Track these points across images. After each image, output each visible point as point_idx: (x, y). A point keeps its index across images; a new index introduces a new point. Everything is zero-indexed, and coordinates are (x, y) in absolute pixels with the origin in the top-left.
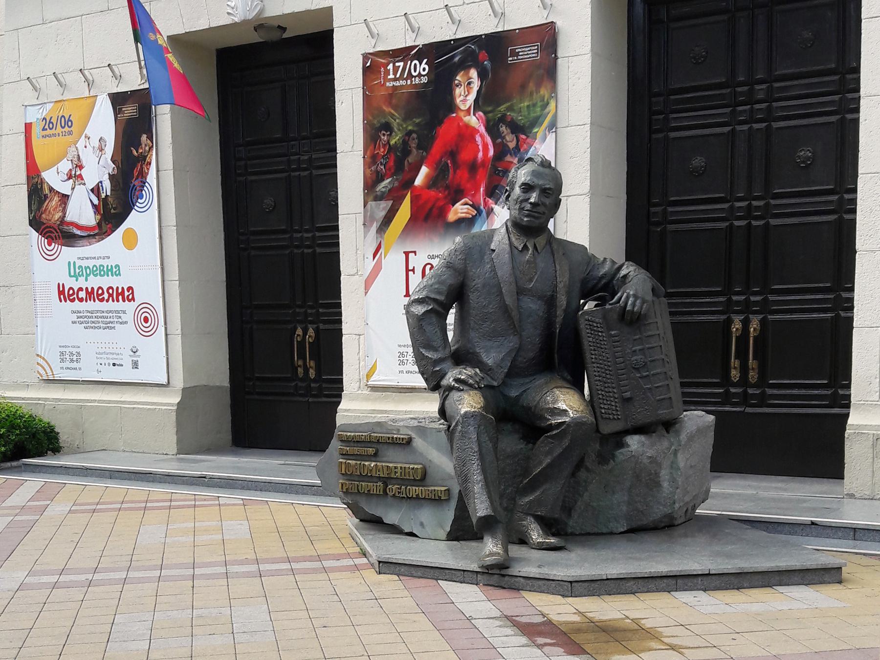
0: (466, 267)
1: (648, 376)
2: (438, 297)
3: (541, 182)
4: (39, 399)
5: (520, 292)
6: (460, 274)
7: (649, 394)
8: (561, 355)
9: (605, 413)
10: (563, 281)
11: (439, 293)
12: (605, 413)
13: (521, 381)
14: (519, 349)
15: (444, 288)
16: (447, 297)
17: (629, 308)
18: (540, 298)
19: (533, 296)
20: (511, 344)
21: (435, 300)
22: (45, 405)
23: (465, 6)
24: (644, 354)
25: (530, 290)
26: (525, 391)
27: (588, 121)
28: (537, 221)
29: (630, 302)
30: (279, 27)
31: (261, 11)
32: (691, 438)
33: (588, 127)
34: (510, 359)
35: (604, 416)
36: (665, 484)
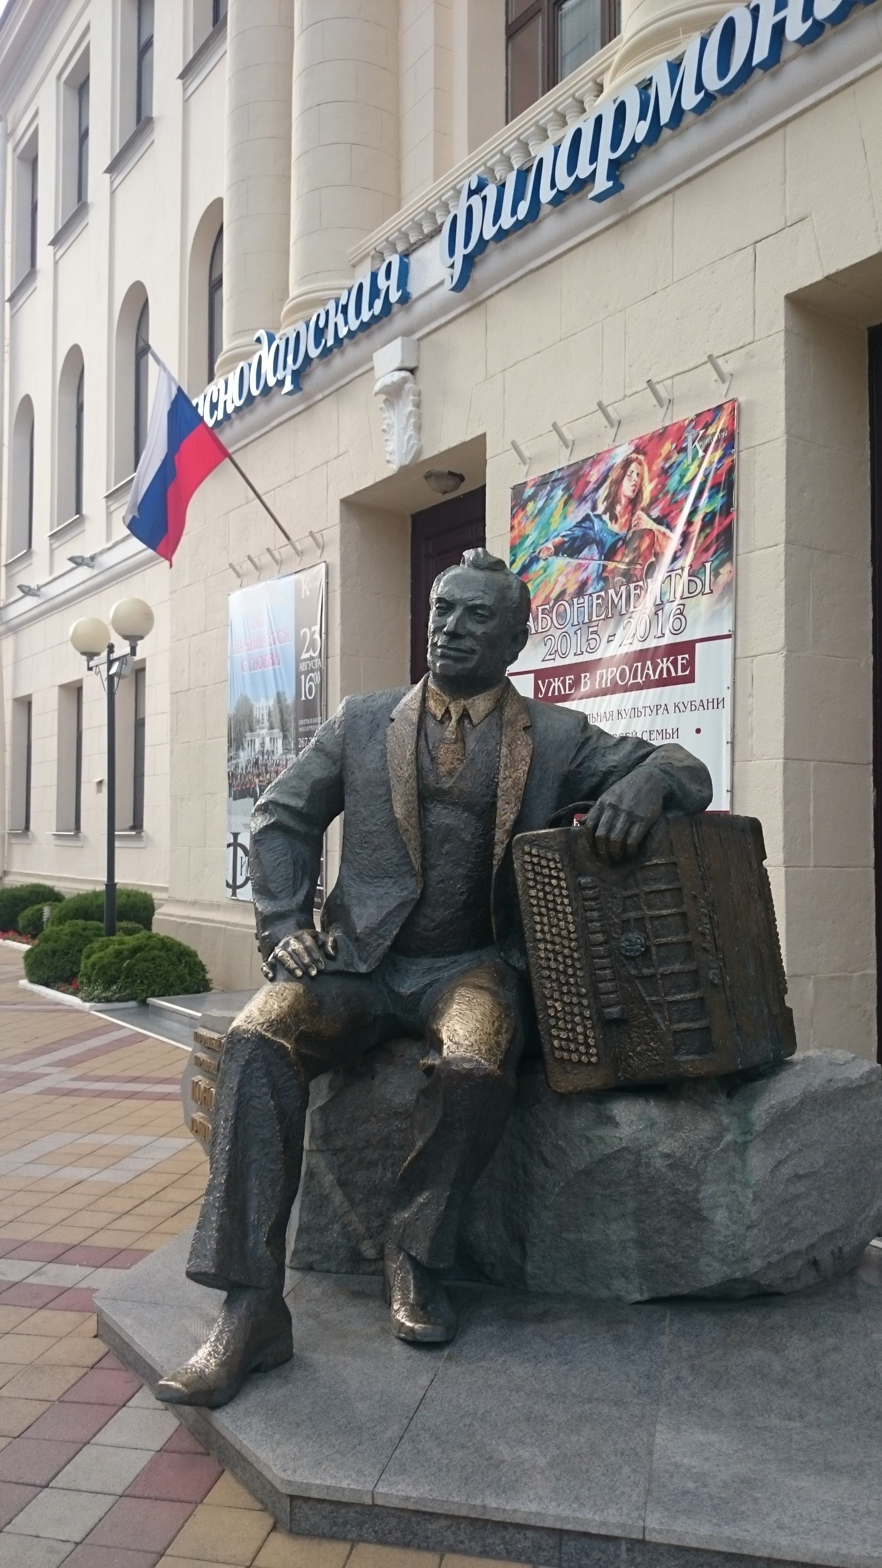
0: (344, 750)
1: (653, 975)
2: (294, 802)
3: (467, 595)
4: (227, 923)
5: (425, 796)
6: (334, 763)
7: (657, 1016)
8: (479, 919)
9: (561, 1048)
10: (512, 777)
11: (298, 795)
12: (561, 1048)
13: (426, 962)
14: (420, 903)
15: (305, 787)
16: (309, 801)
17: (601, 832)
18: (468, 807)
19: (454, 804)
20: (405, 893)
21: (286, 807)
22: (225, 930)
23: (627, 399)
24: (643, 930)
25: (448, 792)
26: (430, 984)
27: (782, 538)
28: (460, 666)
29: (603, 819)
30: (451, 474)
31: (419, 452)
32: (785, 1118)
33: (781, 548)
34: (400, 920)
35: (557, 1054)
36: (720, 1216)
